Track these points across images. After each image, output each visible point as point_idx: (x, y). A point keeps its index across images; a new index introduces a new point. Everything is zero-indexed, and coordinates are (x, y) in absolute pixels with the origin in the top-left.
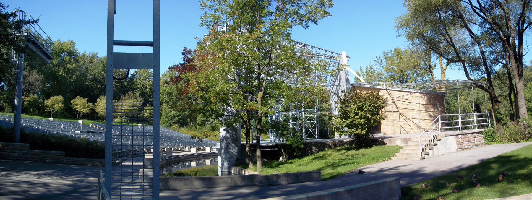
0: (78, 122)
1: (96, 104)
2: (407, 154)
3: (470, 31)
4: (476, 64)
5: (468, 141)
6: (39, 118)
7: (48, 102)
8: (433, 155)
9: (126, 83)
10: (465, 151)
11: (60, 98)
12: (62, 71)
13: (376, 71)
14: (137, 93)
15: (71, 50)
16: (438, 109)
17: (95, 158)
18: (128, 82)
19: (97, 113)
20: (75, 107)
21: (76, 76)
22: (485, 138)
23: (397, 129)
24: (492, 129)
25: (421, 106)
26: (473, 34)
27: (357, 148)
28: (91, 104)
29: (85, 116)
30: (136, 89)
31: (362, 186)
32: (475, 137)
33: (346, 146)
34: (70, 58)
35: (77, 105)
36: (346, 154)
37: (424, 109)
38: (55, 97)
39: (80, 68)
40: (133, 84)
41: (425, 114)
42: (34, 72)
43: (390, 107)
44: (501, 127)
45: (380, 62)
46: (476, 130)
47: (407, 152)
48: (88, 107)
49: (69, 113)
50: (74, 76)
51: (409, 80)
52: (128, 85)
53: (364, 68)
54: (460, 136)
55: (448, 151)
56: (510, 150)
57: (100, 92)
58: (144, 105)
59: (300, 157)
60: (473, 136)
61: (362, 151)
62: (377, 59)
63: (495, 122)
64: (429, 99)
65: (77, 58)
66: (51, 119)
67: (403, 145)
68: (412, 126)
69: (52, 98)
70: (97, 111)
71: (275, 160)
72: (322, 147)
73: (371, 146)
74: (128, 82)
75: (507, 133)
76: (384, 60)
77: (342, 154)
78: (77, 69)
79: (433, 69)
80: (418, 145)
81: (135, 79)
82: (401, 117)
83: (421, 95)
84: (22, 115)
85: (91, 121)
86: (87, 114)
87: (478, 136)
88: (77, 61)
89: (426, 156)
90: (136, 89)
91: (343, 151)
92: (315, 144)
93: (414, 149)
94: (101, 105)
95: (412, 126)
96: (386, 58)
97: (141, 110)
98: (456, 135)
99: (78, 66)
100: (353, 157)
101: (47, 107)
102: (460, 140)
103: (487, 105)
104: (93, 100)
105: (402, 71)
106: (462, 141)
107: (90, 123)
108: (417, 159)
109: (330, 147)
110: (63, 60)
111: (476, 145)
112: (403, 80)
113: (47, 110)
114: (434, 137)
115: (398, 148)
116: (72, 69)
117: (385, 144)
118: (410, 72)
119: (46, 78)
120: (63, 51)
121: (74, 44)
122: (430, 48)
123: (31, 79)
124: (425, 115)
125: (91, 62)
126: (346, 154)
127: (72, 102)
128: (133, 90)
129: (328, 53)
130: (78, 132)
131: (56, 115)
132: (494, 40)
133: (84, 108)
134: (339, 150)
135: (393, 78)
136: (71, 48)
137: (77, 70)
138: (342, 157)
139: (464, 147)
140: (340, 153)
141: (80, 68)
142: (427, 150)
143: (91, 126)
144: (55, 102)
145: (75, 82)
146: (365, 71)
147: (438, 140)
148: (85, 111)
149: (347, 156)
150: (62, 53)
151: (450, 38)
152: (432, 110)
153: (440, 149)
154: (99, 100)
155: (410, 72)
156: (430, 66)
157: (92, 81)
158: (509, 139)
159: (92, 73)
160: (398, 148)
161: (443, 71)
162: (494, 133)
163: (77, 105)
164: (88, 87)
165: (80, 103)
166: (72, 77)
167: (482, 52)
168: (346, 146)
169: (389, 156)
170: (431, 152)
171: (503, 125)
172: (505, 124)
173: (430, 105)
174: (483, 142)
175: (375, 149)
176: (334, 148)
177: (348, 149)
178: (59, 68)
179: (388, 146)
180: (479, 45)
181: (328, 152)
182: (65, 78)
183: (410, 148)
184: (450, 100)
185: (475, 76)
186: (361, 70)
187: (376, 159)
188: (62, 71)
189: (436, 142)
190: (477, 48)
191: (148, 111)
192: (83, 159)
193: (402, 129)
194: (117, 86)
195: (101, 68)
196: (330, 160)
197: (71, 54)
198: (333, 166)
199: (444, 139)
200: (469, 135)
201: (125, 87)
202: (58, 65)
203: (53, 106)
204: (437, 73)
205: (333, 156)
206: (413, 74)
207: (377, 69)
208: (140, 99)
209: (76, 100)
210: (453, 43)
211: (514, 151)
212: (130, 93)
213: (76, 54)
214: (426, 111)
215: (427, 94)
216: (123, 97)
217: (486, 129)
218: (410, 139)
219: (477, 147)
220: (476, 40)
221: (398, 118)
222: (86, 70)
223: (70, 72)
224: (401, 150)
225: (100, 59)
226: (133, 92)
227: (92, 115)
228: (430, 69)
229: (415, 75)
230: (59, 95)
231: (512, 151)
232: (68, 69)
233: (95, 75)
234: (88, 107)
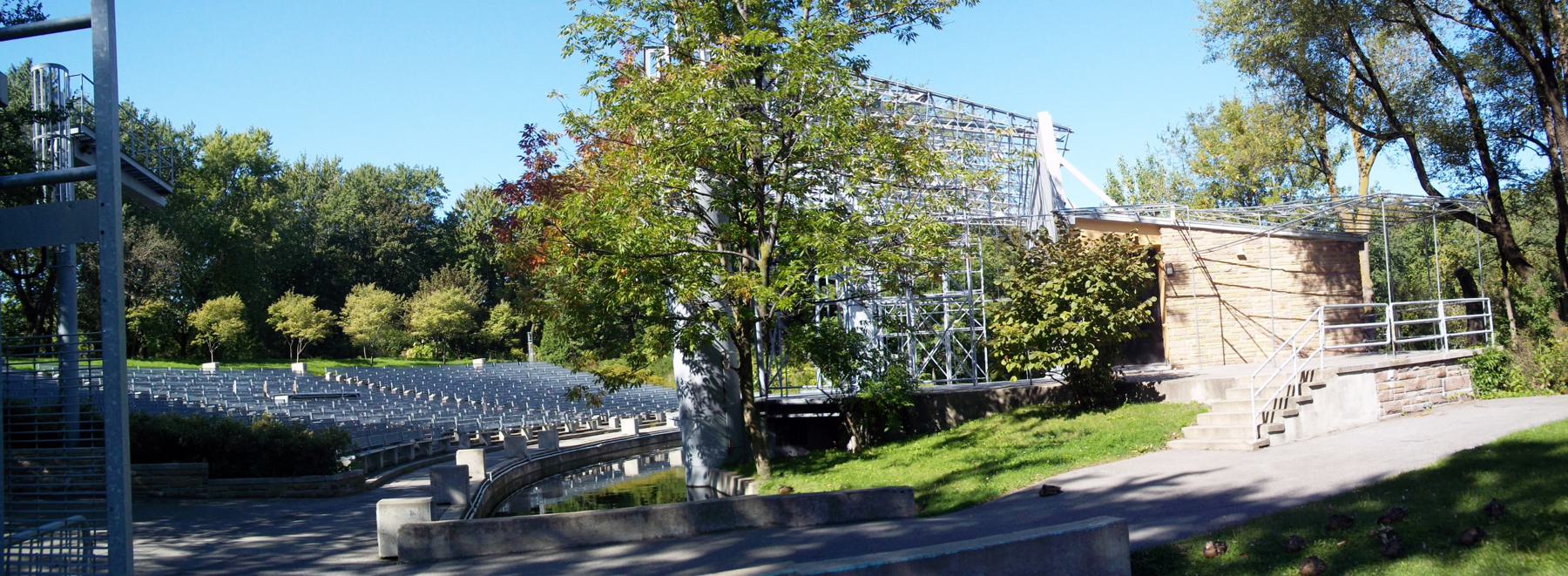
0: (289, 371)
1: (344, 311)
2: (1217, 430)
3: (1431, 38)
4: (1456, 144)
5: (1419, 389)
6: (171, 365)
7: (199, 318)
8: (1298, 435)
9: (433, 241)
10: (1406, 420)
11: (232, 302)
12: (236, 221)
13: (1169, 169)
14: (469, 268)
15: (258, 158)
16: (1342, 287)
17: (299, 474)
18: (440, 236)
19: (348, 337)
20: (280, 326)
21: (281, 234)
22: (1475, 377)
23: (1214, 350)
24: (1501, 348)
25: (1290, 279)
26: (1443, 49)
27: (1073, 413)
28: (326, 313)
29: (314, 350)
30: (465, 255)
31: (981, 546)
32: (1442, 376)
33: (1046, 404)
34: (259, 182)
35: (285, 319)
36: (1037, 429)
37: (1300, 288)
38: (217, 302)
39: (295, 206)
40: (453, 242)
41: (1301, 301)
42: (152, 231)
43: (1197, 282)
44: (1528, 343)
45: (1178, 144)
46: (1445, 353)
47: (1218, 423)
48: (318, 320)
49: (268, 346)
50: (274, 234)
51: (1265, 199)
52: (440, 245)
53: (1131, 163)
54: (1391, 373)
55: (1350, 422)
56: (1545, 420)
57: (358, 274)
58: (492, 301)
59: (904, 438)
60: (1436, 371)
61: (1086, 420)
62: (1168, 136)
63: (1512, 325)
64: (1314, 258)
65: (279, 177)
66: (209, 367)
67: (1209, 402)
68: (1259, 338)
69: (209, 303)
70: (346, 330)
71: (830, 446)
72: (975, 405)
73: (1113, 405)
74: (440, 236)
75: (1546, 361)
76: (1190, 137)
77: (1024, 430)
78: (284, 209)
79: (1336, 163)
80: (1247, 403)
81: (458, 228)
82: (1226, 315)
83: (1288, 244)
84: (130, 362)
85: (333, 364)
86: (317, 341)
87: (1455, 369)
88: (281, 188)
89: (1274, 439)
90: (465, 255)
91: (1034, 420)
92: (956, 399)
93: (1238, 416)
94: (364, 309)
95: (1259, 338)
96: (1195, 133)
97: (481, 316)
98: (1376, 371)
99: (287, 200)
100: (1054, 440)
101: (193, 331)
102: (1391, 384)
103: (1489, 278)
104: (332, 298)
105: (1243, 170)
106: (1400, 391)
107: (325, 368)
108: (1244, 447)
109: (1000, 409)
110: (238, 189)
111: (1445, 401)
112: (1248, 196)
113: (198, 340)
114: (1304, 377)
115: (1193, 412)
116: (267, 212)
117: (1157, 398)
118: (1269, 174)
119: (191, 245)
120: (233, 162)
121: (268, 138)
122: (1308, 95)
123: (142, 253)
124: (1298, 305)
125: (324, 187)
126: (1037, 429)
127: (270, 310)
128: (453, 258)
129: (998, 118)
130: (282, 399)
131: (224, 353)
132: (1512, 69)
133: (307, 325)
134: (1020, 418)
135: (1216, 192)
136: (260, 152)
137: (284, 215)
138: (1020, 439)
139: (1405, 408)
140: (1019, 426)
141: (295, 206)
142: (1278, 420)
143: (328, 377)
144: (219, 315)
145: (279, 248)
146: (1133, 173)
147: (1313, 387)
148: (309, 333)
149: (1037, 435)
150: (234, 168)
151: (1365, 61)
152: (1324, 289)
153: (1323, 413)
154: (350, 299)
155: (1269, 174)
156: (1324, 152)
157: (330, 243)
158: (1552, 382)
159: (331, 218)
160: (1193, 412)
161: (1365, 169)
162: (1504, 361)
163: (285, 319)
164: (320, 264)
165: (294, 312)
166: (267, 237)
167: (1472, 107)
168: (1046, 404)
169: (1160, 440)
170: (1289, 424)
171: (1535, 335)
172: (1545, 332)
173: (1318, 273)
174: (1469, 389)
175: (1128, 415)
176: (1010, 413)
177: (1045, 415)
178: (227, 213)
179: (1166, 406)
180: (1462, 82)
181: (993, 420)
182: (249, 241)
183: (1230, 411)
184: (1408, 256)
185: (1448, 184)
186: (1123, 167)
187: (1119, 447)
188: (236, 221)
189: (1307, 392)
190: (1453, 93)
191: (499, 321)
192: (261, 479)
193: (1228, 349)
194: (405, 251)
195: (353, 201)
196: (983, 450)
197: (261, 167)
198: (990, 468)
199: (1334, 383)
200: (1422, 370)
201: (432, 252)
202: (222, 205)
203: (214, 327)
204: (1347, 175)
205: (998, 434)
206: (1281, 181)
207: (1173, 164)
208: (476, 285)
209: (282, 303)
210: (1373, 78)
211: (1551, 426)
212: (443, 270)
213: (277, 168)
214: (1305, 294)
215: (1306, 240)
216: (424, 284)
217: (1479, 350)
218: (1231, 383)
219: (1445, 407)
220: (1452, 67)
221: (1215, 316)
222: (313, 213)
223: (265, 222)
224: (1200, 418)
225: (350, 177)
226: (452, 266)
227: (335, 345)
228: (1322, 166)
229: (1287, 181)
230: (228, 293)
231: (1545, 426)
232: (255, 212)
233: (338, 223)
234: (318, 320)
